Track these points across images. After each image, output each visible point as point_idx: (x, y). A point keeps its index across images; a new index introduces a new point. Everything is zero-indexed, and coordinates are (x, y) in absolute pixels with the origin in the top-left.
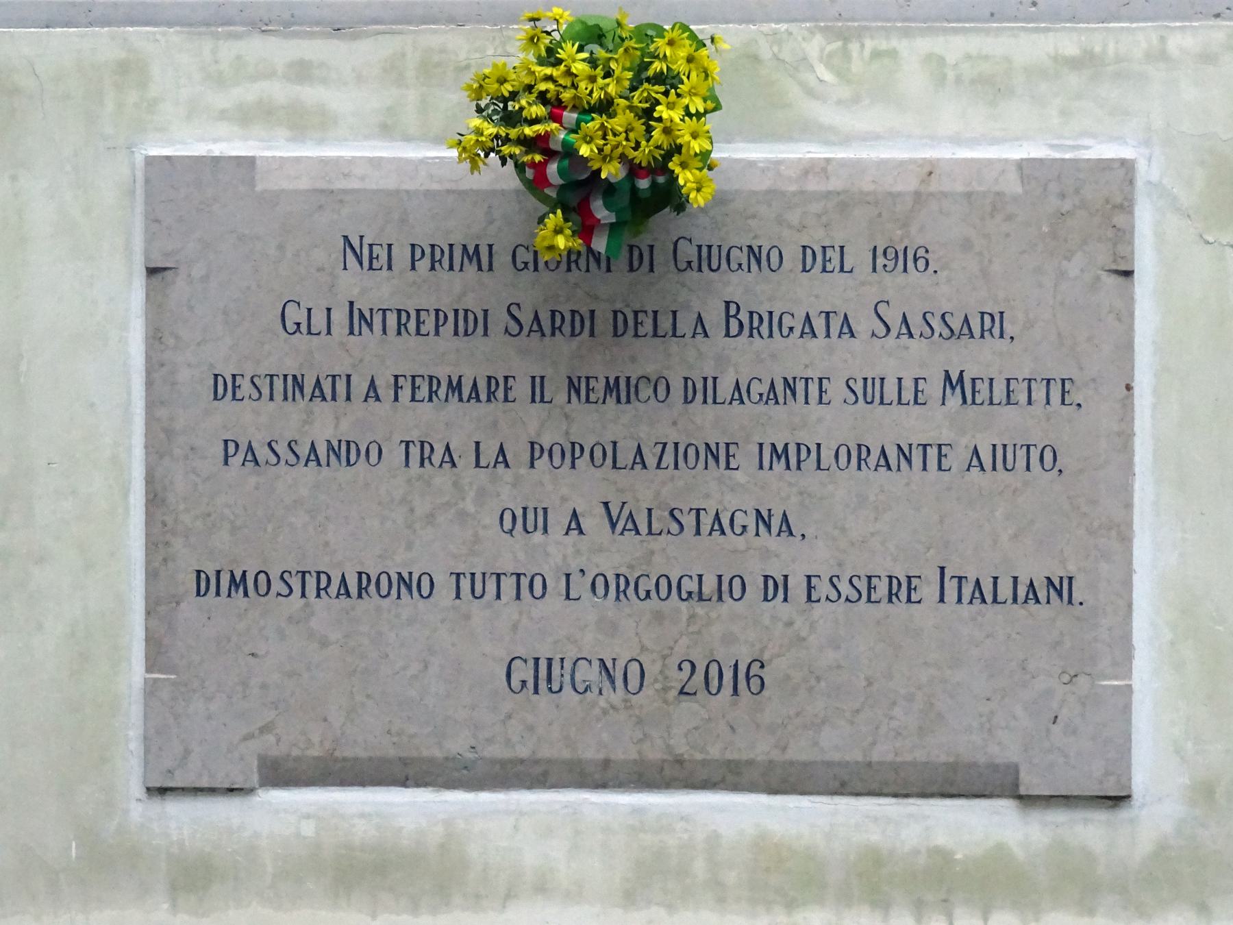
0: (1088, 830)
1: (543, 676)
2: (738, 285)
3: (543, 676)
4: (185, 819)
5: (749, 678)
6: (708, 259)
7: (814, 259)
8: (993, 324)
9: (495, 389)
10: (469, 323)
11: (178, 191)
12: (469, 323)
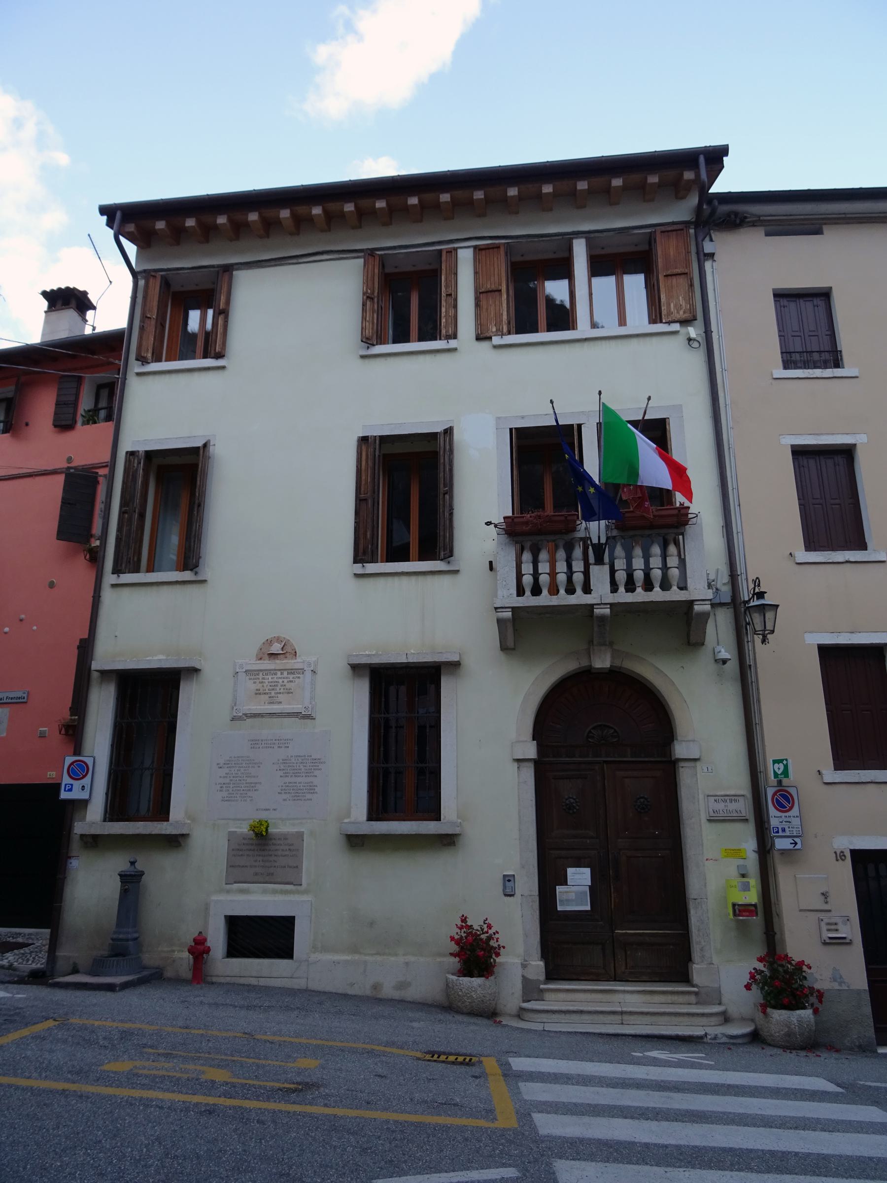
0: (299, 887)
1: (256, 874)
2: (273, 841)
3: (256, 874)
4: (228, 886)
5: (272, 874)
6: (271, 839)
7: (280, 839)
8: (292, 845)
9: (254, 850)
10: (252, 844)
11: (231, 834)
12: (252, 844)
